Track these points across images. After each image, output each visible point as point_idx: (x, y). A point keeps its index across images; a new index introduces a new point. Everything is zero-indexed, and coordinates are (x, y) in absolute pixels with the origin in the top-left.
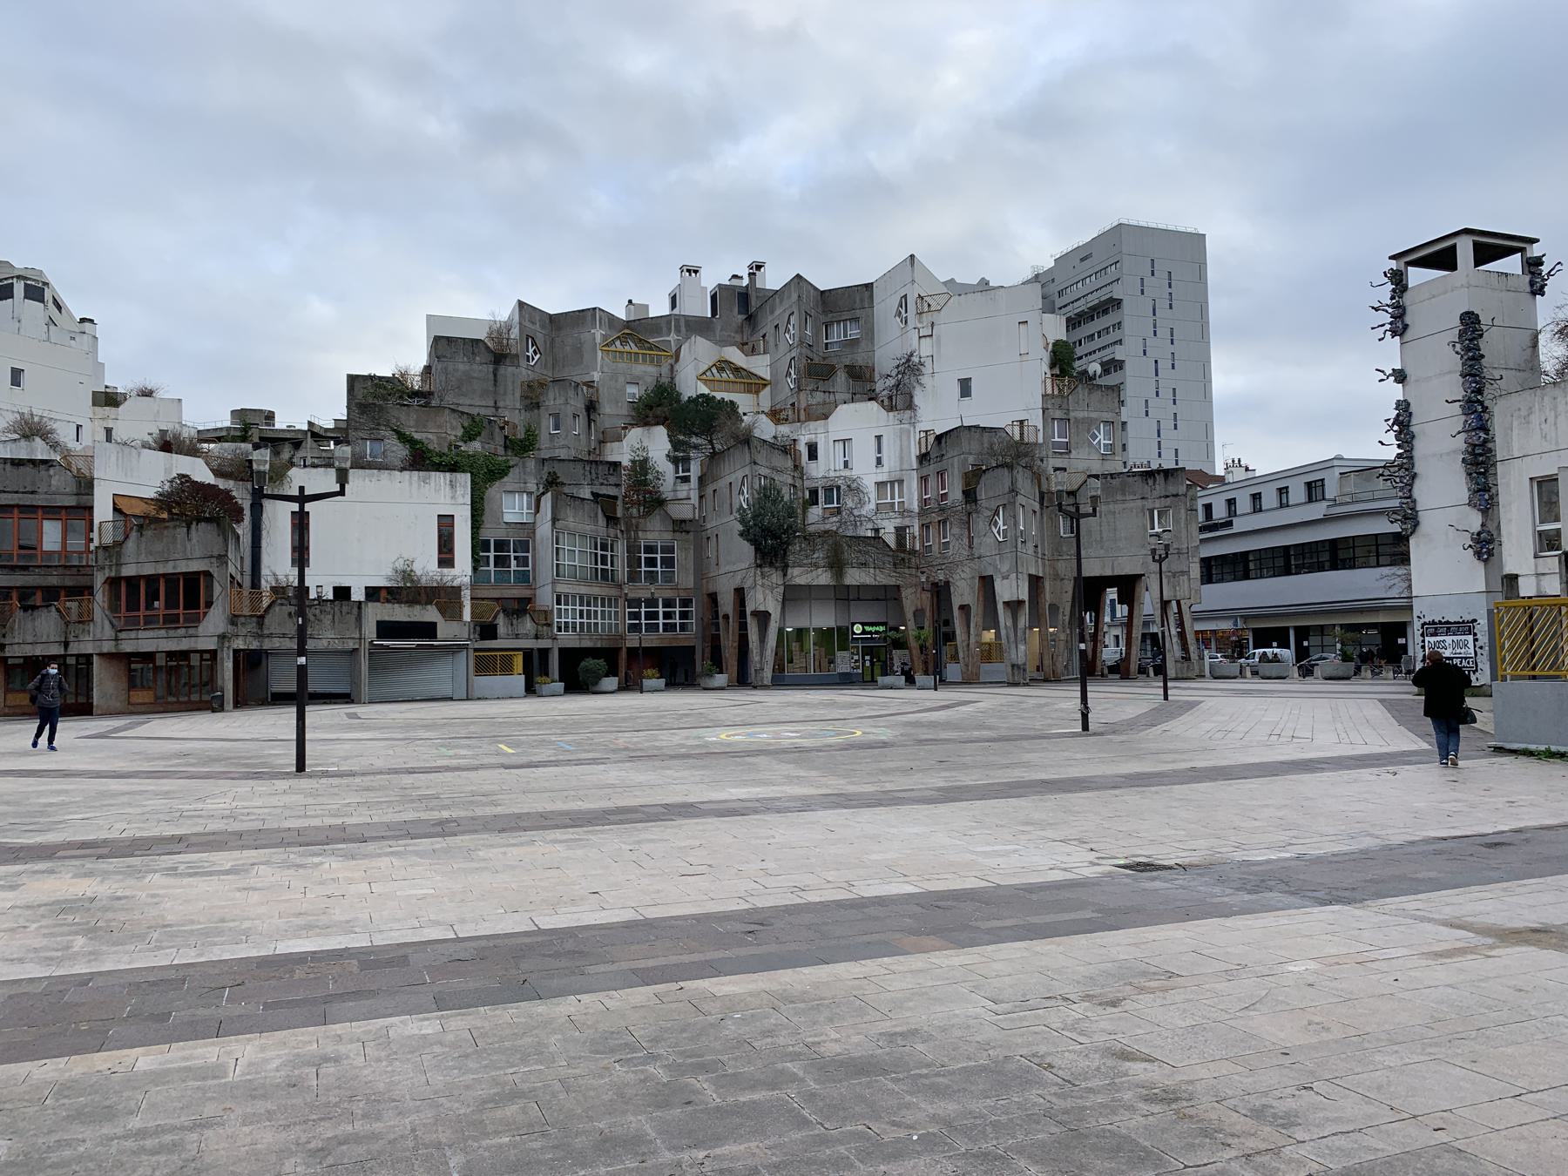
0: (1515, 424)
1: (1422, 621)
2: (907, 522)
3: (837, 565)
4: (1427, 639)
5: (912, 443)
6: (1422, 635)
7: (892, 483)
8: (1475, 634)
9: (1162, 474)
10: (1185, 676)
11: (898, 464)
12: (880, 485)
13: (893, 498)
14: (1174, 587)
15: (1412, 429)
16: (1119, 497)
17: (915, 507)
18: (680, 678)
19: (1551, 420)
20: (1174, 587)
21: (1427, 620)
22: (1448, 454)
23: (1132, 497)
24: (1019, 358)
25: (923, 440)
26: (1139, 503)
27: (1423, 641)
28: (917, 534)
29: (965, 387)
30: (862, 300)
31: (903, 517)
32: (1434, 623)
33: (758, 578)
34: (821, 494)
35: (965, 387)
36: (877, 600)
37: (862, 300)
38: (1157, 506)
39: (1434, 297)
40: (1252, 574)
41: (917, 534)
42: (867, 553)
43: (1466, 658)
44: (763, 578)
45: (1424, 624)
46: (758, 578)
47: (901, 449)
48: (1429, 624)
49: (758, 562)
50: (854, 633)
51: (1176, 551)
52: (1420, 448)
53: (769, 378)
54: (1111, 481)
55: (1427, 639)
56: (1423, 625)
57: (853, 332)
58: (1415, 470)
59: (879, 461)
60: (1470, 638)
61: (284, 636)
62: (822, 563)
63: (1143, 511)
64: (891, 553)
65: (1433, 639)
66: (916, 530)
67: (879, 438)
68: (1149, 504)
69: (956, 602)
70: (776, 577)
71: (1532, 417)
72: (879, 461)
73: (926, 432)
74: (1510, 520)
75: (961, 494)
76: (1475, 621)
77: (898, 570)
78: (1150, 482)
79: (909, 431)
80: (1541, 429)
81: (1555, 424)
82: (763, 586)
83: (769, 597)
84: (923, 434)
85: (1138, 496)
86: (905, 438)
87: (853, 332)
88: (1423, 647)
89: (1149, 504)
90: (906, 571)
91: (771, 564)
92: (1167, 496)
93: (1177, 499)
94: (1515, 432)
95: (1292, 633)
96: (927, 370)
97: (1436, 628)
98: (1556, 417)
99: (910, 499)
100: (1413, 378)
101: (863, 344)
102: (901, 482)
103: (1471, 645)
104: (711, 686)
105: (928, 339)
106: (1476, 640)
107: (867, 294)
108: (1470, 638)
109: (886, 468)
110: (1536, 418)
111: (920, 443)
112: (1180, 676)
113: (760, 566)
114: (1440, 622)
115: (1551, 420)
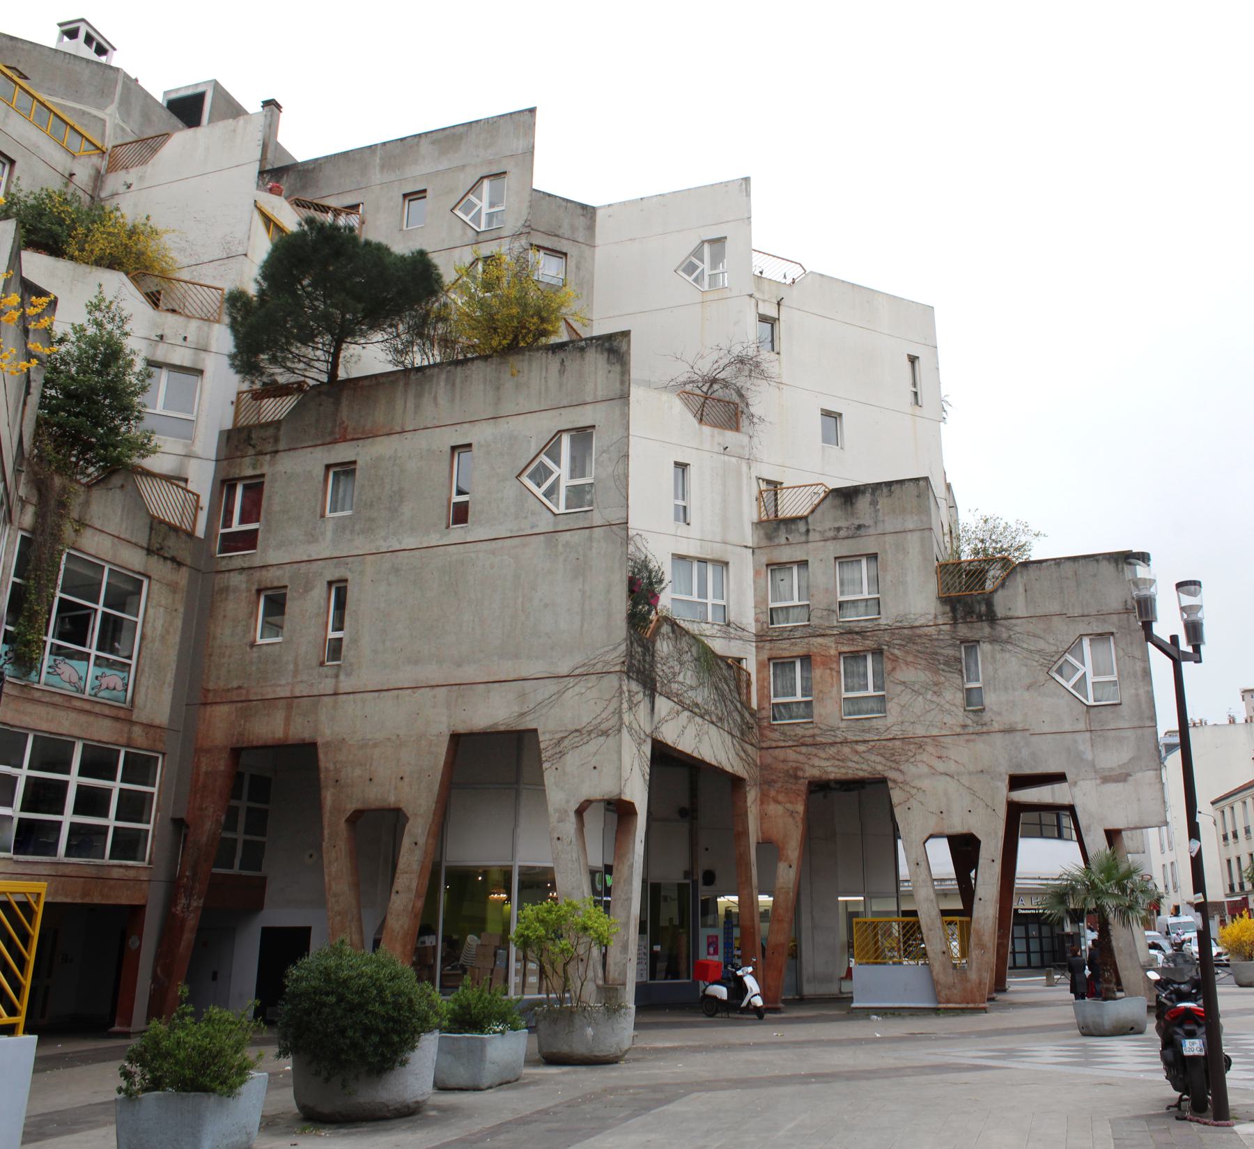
13: (703, 593)
30: (573, 228)
72: (683, 514)
107: (581, 222)
109: (694, 530)
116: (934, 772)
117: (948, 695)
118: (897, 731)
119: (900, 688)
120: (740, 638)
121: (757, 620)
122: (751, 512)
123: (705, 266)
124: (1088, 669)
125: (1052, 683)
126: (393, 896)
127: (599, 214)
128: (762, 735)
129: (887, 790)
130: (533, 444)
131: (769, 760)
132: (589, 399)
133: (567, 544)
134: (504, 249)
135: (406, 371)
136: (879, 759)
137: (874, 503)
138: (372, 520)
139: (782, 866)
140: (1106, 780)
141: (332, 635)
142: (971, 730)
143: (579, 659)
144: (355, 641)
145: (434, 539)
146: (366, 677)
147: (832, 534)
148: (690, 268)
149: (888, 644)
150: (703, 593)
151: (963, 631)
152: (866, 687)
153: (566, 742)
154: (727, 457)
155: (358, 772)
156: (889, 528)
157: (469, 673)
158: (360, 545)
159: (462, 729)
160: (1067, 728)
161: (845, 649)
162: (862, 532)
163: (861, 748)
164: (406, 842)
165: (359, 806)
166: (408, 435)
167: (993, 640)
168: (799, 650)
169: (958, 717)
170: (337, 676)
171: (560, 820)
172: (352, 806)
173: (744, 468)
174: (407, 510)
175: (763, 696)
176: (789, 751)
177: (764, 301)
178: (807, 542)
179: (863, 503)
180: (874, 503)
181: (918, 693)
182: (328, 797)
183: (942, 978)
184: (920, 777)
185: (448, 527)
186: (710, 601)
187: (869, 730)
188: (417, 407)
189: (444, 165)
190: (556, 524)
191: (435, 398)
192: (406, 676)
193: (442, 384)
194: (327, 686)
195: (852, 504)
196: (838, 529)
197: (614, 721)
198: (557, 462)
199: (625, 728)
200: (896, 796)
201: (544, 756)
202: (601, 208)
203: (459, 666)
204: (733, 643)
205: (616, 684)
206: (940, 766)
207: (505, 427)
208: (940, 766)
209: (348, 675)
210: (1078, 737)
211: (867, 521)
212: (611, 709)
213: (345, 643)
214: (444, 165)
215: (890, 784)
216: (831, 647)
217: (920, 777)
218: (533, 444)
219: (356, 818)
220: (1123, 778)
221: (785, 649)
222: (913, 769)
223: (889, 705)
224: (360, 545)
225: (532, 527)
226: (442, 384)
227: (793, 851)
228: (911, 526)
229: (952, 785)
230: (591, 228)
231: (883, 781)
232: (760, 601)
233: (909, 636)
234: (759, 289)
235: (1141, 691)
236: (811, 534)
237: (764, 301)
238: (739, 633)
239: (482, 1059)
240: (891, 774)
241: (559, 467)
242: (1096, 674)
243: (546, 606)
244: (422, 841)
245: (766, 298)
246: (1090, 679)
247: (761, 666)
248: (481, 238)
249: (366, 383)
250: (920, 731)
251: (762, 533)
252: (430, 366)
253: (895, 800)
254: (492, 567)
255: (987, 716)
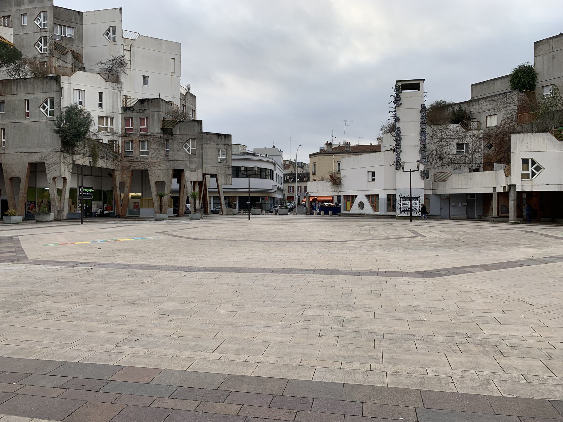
0: (518, 142)
1: (401, 196)
2: (115, 138)
3: (94, 155)
4: (402, 202)
5: (119, 100)
6: (400, 201)
7: (107, 118)
8: (419, 201)
9: (224, 136)
10: (229, 214)
11: (111, 109)
12: (101, 118)
13: (107, 124)
14: (226, 180)
15: (401, 136)
16: (209, 142)
17: (120, 131)
18: (477, 212)
19: (529, 143)
20: (226, 180)
21: (402, 196)
22: (413, 146)
23: (213, 143)
24: (170, 74)
25: (125, 100)
26: (216, 146)
27: (401, 203)
28: (120, 145)
29: (145, 79)
30: (76, 19)
31: (113, 136)
32: (405, 197)
33: (62, 158)
34: (423, 130)
35: (145, 79)
36: (98, 176)
37: (76, 19)
38: (222, 148)
39: (411, 97)
40: (262, 176)
41: (120, 145)
42: (104, 151)
43: (416, 208)
44: (64, 159)
45: (402, 197)
46: (62, 158)
47: (113, 102)
48: (403, 197)
49: (62, 149)
50: (80, 192)
51: (227, 166)
52: (403, 143)
53: (12, 42)
54: (206, 135)
55: (402, 202)
56: (401, 198)
57: (69, 32)
58: (401, 149)
59: (100, 105)
60: (418, 202)
61: (206, 170)
62: (88, 154)
63: (217, 149)
64: (112, 153)
65: (404, 202)
66: (120, 143)
67: (100, 94)
68: (219, 147)
69: (153, 180)
70: (69, 160)
71: (523, 141)
72: (100, 105)
73: (126, 96)
74: (514, 169)
75: (160, 130)
76: (420, 197)
77: (115, 162)
78: (220, 138)
79: (117, 94)
80: (526, 145)
81: (531, 144)
82: (64, 163)
83: (66, 170)
84: (124, 97)
85: (215, 143)
86: (115, 97)
87: (69, 32)
88: (400, 205)
89: (219, 147)
90: (117, 162)
91: (67, 152)
92: (225, 145)
93: (228, 146)
94: (518, 145)
95: (238, 198)
96: (128, 66)
97: (406, 199)
98: (531, 142)
99: (117, 127)
100: (402, 121)
101: (76, 42)
102: (112, 118)
103: (418, 204)
104: (47, 220)
105: (128, 51)
106: (419, 203)
107: (78, 17)
108: (418, 202)
109: (104, 110)
110: (524, 142)
111: (123, 101)
112: (227, 214)
113: (62, 152)
114: (407, 197)
115: (529, 143)
116: (158, 169)
117: (162, 152)
118: (150, 159)
119: (152, 149)
120: (117, 136)
121: (121, 132)
122: (120, 105)
123: (111, 34)
124: (190, 146)
125: (183, 149)
126: (20, 194)
127: (84, 14)
128: (122, 159)
129: (148, 172)
130: (42, 100)
131: (124, 165)
132: (53, 91)
133: (49, 124)
134: (48, 35)
135: (14, 79)
136: (147, 165)
137: (148, 104)
138: (9, 115)
139: (126, 187)
140: (191, 171)
141: (3, 140)
142: (166, 160)
143: (52, 148)
144: (7, 142)
145: (22, 121)
146: (10, 150)
147: (138, 111)
148: (107, 34)
149: (150, 139)
150: (107, 124)
151: (165, 136)
152: (145, 149)
153: (50, 165)
154: (114, 90)
155: (10, 170)
156: (151, 111)
157: (31, 150)
158: (7, 121)
159: (30, 162)
160: (185, 159)
161: (140, 139)
162: (145, 111)
163: (143, 163)
164: (21, 184)
165: (11, 177)
166: (15, 95)
167: (172, 139)
168: (130, 139)
169: (163, 157)
170: (5, 149)
171: (50, 181)
172: (10, 177)
173: (119, 93)
174: (16, 113)
175: (123, 150)
176: (128, 163)
177: (126, 45)
178: (133, 113)
179: (146, 103)
180: (148, 104)
181: (155, 151)
182: (5, 174)
183: (157, 211)
184: (155, 170)
185: (25, 118)
186: (109, 127)
187: (145, 159)
188: (17, 89)
189: (31, 7)
190: (47, 119)
191: (20, 87)
192: (19, 150)
193: (22, 84)
194: (3, 151)
195: (143, 104)
196: (140, 110)
197: (59, 161)
198: (47, 105)
199: (62, 163)
200: (150, 174)
201: (46, 168)
202: (84, 12)
203: (29, 149)
204: (115, 137)
205: (59, 154)
206: (159, 168)
207: (36, 95)
208: (159, 168)
209: (7, 149)
210: (187, 161)
211: (147, 109)
212: (58, 159)
213: (6, 142)
214: (31, 7)
215: (149, 171)
216: (137, 139)
217: (155, 170)
218: (42, 100)
219: (11, 179)
220: (195, 171)
221: (128, 139)
222: (153, 168)
223: (149, 153)
224: (7, 121)
225: (42, 119)
226: (22, 84)
227: (128, 184)
228: (156, 111)
229: (161, 172)
230: (81, 19)
231: (147, 170)
232: (122, 127)
233: (153, 136)
234: (124, 42)
235: (200, 152)
236: (134, 111)
237: (126, 45)
238: (117, 135)
239: (11, 220)
240: (149, 169)
241: (47, 105)
242: (192, 148)
243: (46, 137)
244: (24, 183)
245: (127, 44)
246: (191, 149)
247: (122, 143)
248: (42, 31)
249: (5, 81)
250: (155, 159)
251: (123, 110)
252: (19, 79)
253: (149, 175)
254: (35, 127)
255: (169, 157)
